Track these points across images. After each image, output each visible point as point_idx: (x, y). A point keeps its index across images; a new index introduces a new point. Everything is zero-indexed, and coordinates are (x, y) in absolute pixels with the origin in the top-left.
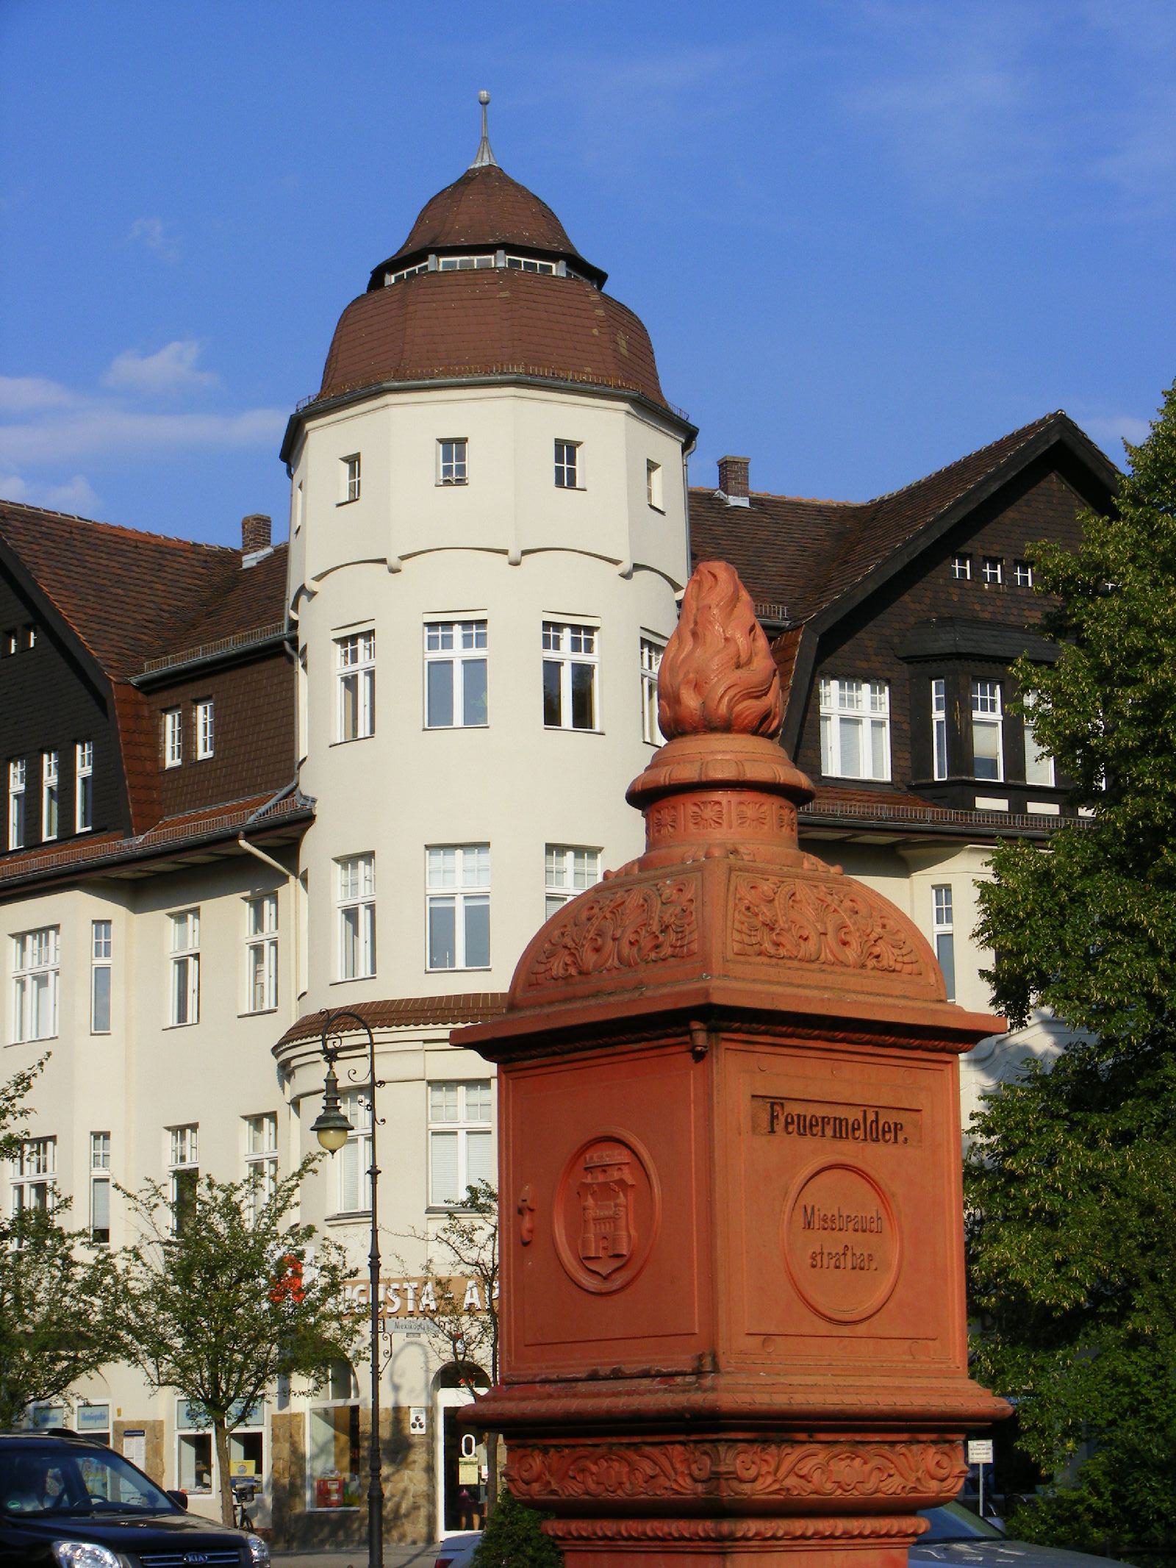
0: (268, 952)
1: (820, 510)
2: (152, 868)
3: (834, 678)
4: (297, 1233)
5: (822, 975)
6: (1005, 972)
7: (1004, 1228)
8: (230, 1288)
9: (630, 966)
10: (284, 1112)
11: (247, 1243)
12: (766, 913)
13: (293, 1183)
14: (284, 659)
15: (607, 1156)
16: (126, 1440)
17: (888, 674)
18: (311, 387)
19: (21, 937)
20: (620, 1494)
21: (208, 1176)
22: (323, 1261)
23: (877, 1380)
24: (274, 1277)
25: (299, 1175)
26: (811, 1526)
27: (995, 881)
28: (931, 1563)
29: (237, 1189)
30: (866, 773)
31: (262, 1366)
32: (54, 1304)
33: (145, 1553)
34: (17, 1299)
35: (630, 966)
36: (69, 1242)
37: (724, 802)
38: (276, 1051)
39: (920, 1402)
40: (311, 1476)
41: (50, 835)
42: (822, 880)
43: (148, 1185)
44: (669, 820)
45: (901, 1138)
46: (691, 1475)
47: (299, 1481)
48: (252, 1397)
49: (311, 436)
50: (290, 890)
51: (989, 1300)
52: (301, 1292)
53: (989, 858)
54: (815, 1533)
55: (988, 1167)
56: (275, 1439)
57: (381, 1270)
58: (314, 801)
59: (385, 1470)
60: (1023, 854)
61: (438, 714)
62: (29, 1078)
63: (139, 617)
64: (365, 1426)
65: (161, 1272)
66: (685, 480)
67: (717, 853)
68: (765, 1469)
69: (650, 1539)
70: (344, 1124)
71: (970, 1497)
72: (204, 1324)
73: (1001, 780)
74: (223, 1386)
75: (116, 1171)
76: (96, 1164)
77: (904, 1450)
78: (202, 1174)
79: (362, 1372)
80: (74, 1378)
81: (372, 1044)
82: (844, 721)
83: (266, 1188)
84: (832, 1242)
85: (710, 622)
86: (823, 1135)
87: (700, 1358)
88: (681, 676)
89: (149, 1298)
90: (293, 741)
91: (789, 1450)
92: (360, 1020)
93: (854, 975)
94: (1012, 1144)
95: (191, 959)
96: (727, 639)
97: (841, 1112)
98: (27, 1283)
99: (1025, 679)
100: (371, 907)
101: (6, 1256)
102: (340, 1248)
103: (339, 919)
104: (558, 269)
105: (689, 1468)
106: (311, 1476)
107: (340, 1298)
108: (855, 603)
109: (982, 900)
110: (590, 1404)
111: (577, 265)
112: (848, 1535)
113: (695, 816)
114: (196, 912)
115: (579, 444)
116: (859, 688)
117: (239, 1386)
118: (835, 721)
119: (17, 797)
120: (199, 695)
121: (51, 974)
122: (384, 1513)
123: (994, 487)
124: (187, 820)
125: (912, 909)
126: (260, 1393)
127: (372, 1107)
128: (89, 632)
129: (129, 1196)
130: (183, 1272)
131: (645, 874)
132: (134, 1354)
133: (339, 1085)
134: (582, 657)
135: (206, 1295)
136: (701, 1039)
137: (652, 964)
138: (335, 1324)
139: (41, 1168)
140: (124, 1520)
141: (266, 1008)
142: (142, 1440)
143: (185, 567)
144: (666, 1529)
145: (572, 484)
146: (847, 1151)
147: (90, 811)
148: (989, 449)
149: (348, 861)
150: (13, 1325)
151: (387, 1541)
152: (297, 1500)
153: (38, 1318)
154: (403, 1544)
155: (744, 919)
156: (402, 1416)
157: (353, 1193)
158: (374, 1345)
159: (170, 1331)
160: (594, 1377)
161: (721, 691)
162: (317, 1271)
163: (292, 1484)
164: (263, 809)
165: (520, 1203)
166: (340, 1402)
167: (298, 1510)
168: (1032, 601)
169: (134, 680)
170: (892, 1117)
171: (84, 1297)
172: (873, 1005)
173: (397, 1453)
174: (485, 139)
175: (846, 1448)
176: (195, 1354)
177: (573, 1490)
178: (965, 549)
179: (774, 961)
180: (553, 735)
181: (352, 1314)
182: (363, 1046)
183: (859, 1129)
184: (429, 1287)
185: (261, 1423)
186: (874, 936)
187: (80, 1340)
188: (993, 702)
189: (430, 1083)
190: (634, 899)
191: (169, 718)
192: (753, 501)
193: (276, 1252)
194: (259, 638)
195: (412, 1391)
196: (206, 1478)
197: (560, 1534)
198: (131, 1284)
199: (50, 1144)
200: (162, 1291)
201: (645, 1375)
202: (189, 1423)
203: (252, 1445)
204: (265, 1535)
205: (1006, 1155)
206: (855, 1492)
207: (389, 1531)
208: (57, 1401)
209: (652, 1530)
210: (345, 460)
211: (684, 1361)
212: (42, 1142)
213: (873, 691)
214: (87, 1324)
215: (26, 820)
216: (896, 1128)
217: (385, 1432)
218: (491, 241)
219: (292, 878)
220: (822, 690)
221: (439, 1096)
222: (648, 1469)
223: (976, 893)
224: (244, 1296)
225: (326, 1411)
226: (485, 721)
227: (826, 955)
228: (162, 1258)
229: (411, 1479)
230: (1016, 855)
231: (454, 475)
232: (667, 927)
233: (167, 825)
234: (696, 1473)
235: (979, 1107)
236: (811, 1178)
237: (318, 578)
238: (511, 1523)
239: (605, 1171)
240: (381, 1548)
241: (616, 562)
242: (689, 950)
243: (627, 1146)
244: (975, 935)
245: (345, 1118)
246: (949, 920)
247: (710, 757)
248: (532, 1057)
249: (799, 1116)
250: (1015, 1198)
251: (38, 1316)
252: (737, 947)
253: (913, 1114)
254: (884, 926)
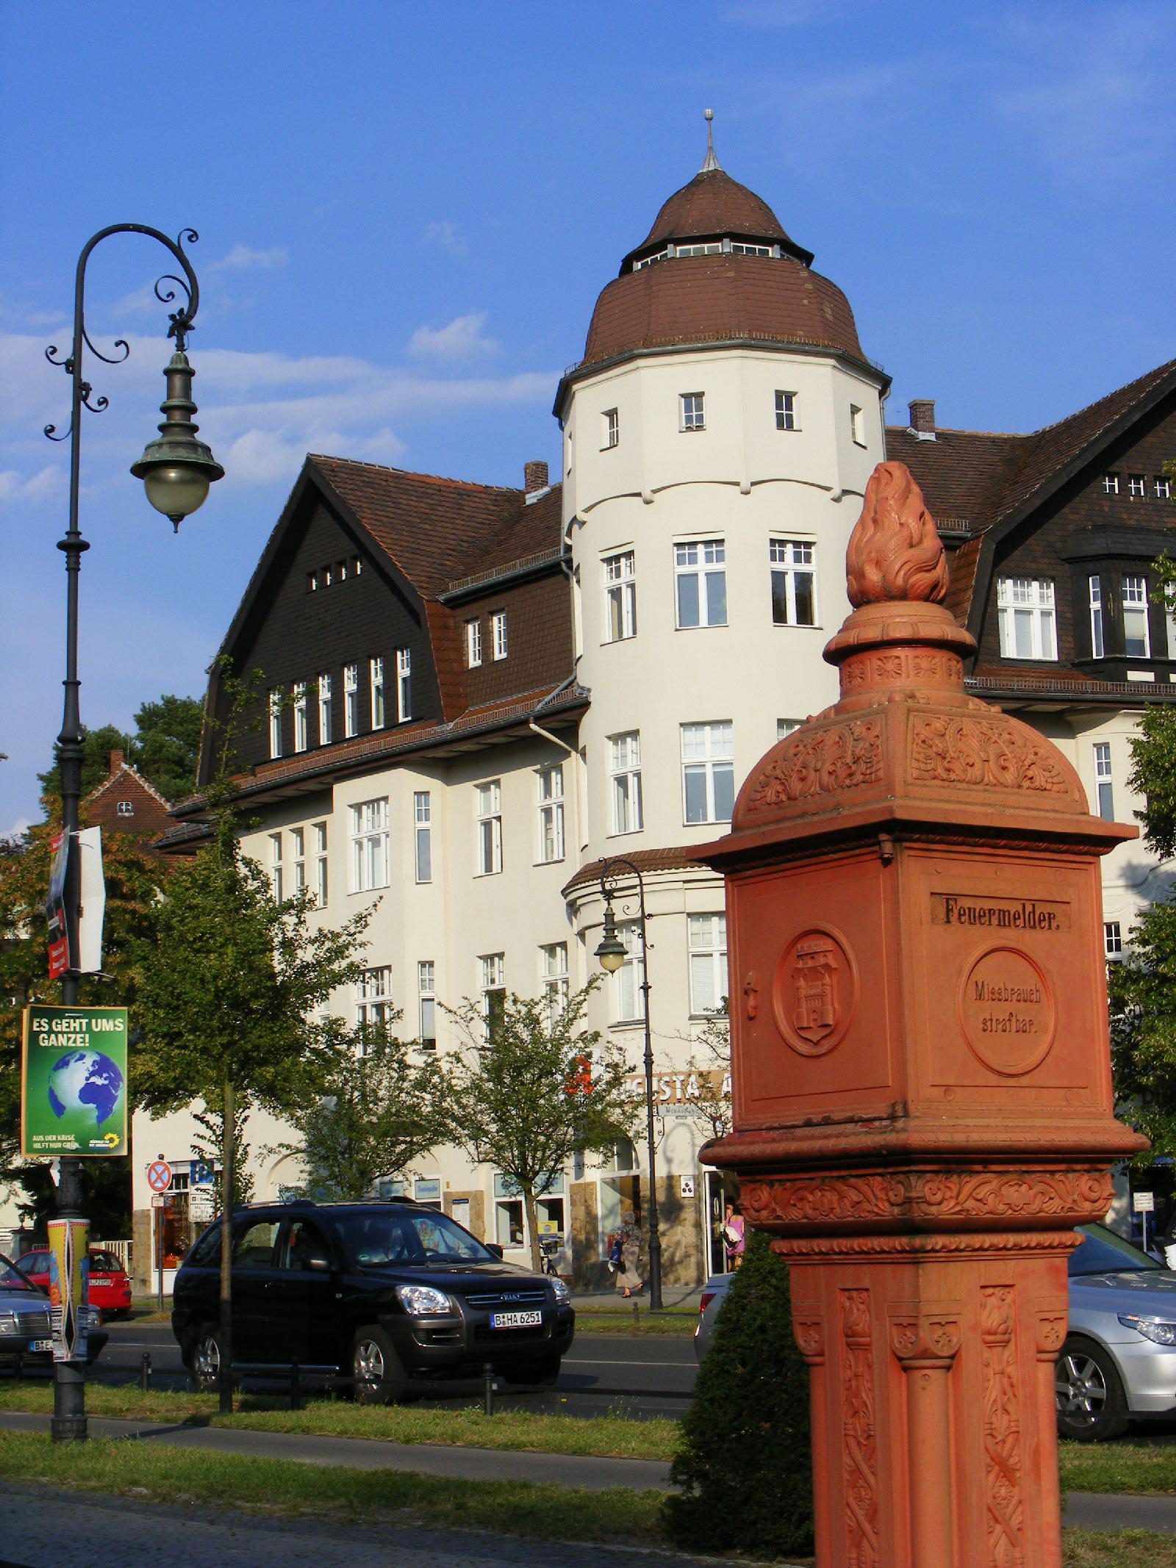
0: (556, 813)
1: (994, 441)
2: (460, 749)
3: (1009, 577)
4: (586, 1038)
5: (987, 795)
6: (1154, 812)
7: (1159, 1021)
8: (533, 1083)
9: (830, 791)
10: (573, 942)
11: (545, 1047)
12: (939, 744)
13: (582, 998)
14: (561, 577)
15: (815, 945)
16: (454, 1207)
17: (1053, 573)
18: (576, 356)
19: (357, 807)
20: (833, 1218)
21: (513, 994)
22: (608, 1060)
23: (1039, 1122)
24: (568, 1074)
25: (586, 991)
26: (988, 1240)
27: (1144, 739)
28: (1107, 1290)
29: (537, 1004)
30: (1037, 654)
31: (560, 1145)
32: (393, 1099)
33: (468, 1295)
34: (364, 1095)
35: (830, 791)
36: (403, 1050)
37: (903, 657)
38: (565, 893)
39: (1077, 1139)
40: (603, 1233)
41: (378, 724)
42: (984, 718)
43: (465, 1003)
44: (858, 671)
45: (1054, 925)
46: (888, 1200)
47: (592, 1237)
48: (553, 1171)
49: (577, 396)
50: (572, 763)
51: (1148, 1079)
52: (590, 1085)
53: (1139, 720)
54: (991, 1246)
55: (1144, 971)
56: (573, 1203)
57: (654, 1066)
58: (589, 690)
59: (662, 1227)
60: (1167, 716)
61: (687, 616)
62: (366, 917)
63: (443, 547)
64: (645, 1191)
65: (478, 1071)
66: (883, 420)
67: (897, 697)
68: (948, 1194)
69: (857, 1253)
70: (621, 949)
71: (1136, 1239)
72: (514, 1112)
73: (1148, 656)
74: (530, 1161)
75: (439, 992)
76: (423, 987)
77: (1062, 1178)
78: (508, 993)
79: (641, 1148)
80: (411, 1158)
81: (641, 885)
82: (1017, 612)
83: (560, 1002)
84: (1001, 1011)
85: (887, 511)
86: (990, 924)
87: (893, 1105)
88: (864, 556)
89: (468, 1093)
90: (571, 650)
91: (968, 1179)
92: (633, 867)
93: (1012, 794)
94: (1164, 952)
95: (494, 821)
96: (901, 525)
97: (1004, 905)
98: (371, 1083)
99: (1165, 572)
100: (638, 775)
101: (353, 1063)
102: (621, 1049)
103: (613, 785)
104: (773, 252)
105: (887, 1195)
106: (603, 1233)
107: (622, 1089)
108: (1024, 515)
109: (1134, 754)
110: (805, 1146)
111: (789, 248)
112: (1018, 1247)
113: (880, 668)
114: (497, 783)
115: (795, 394)
116: (1029, 585)
117: (543, 1161)
118: (1011, 612)
119: (351, 695)
120: (495, 608)
121: (383, 836)
122: (662, 1261)
123: (1136, 418)
124: (488, 709)
125: (1077, 758)
126: (560, 1166)
127: (642, 935)
128: (404, 560)
129: (450, 1011)
130: (495, 1071)
131: (840, 717)
132: (458, 1138)
133: (616, 919)
134: (803, 567)
135: (514, 1090)
136: (888, 848)
137: (846, 790)
138: (618, 1111)
139: (380, 991)
140: (453, 1268)
141: (556, 858)
142: (466, 1206)
143: (480, 505)
144: (870, 1245)
145: (790, 427)
146: (1011, 936)
147: (409, 704)
148: (1131, 387)
149: (618, 738)
150: (361, 1117)
151: (665, 1284)
152: (592, 1252)
153: (380, 1111)
154: (678, 1286)
155: (920, 750)
156: (674, 1183)
157: (631, 1006)
158: (650, 1126)
159: (486, 1118)
160: (809, 1124)
161: (897, 567)
162: (603, 1068)
163: (588, 1239)
164: (547, 699)
165: (746, 986)
166: (624, 1173)
167: (593, 1260)
168: (1169, 509)
169: (441, 598)
170: (1048, 908)
171: (417, 1093)
172: (1028, 817)
173: (672, 1213)
174: (711, 148)
175: (1015, 1176)
176: (507, 1137)
177: (794, 1215)
178: (1111, 469)
179: (946, 784)
180: (781, 631)
181: (631, 1102)
182: (634, 887)
183: (1019, 918)
184: (693, 1078)
185: (562, 1191)
186: (1028, 762)
187: (416, 1128)
188: (1140, 593)
189: (689, 915)
190: (832, 737)
191: (470, 627)
192: (938, 435)
193: (570, 1053)
194: (540, 560)
195: (681, 1162)
196: (519, 1236)
197: (785, 1251)
198: (454, 1082)
199: (386, 972)
200: (478, 1087)
201: (851, 1120)
202: (503, 1192)
203: (555, 1209)
204: (567, 1279)
205: (1159, 961)
206: (1022, 1212)
207: (666, 1275)
208: (397, 1176)
209: (859, 1246)
210: (606, 414)
211: (881, 1109)
212: (378, 972)
213: (1041, 587)
214: (420, 1114)
215: (359, 713)
216: (1049, 918)
217: (661, 1196)
218: (718, 231)
219: (573, 753)
220: (999, 588)
221: (697, 926)
222: (854, 1196)
223: (1130, 748)
224: (544, 1090)
225: (613, 1180)
226: (725, 621)
227: (989, 778)
228: (478, 1060)
229: (683, 1234)
230: (1162, 717)
231: (694, 423)
232: (858, 759)
233: (472, 713)
234: (893, 1199)
235: (1137, 922)
236: (982, 958)
237: (587, 510)
238: (758, 1259)
239: (813, 958)
240: (660, 1290)
241: (828, 489)
242: (876, 776)
243: (834, 939)
244: (1130, 783)
245: (622, 945)
246: (1108, 772)
247: (890, 621)
248: (752, 868)
249: (969, 909)
250: (1167, 995)
251: (380, 1108)
252: (915, 773)
253: (1064, 906)
254: (1036, 754)
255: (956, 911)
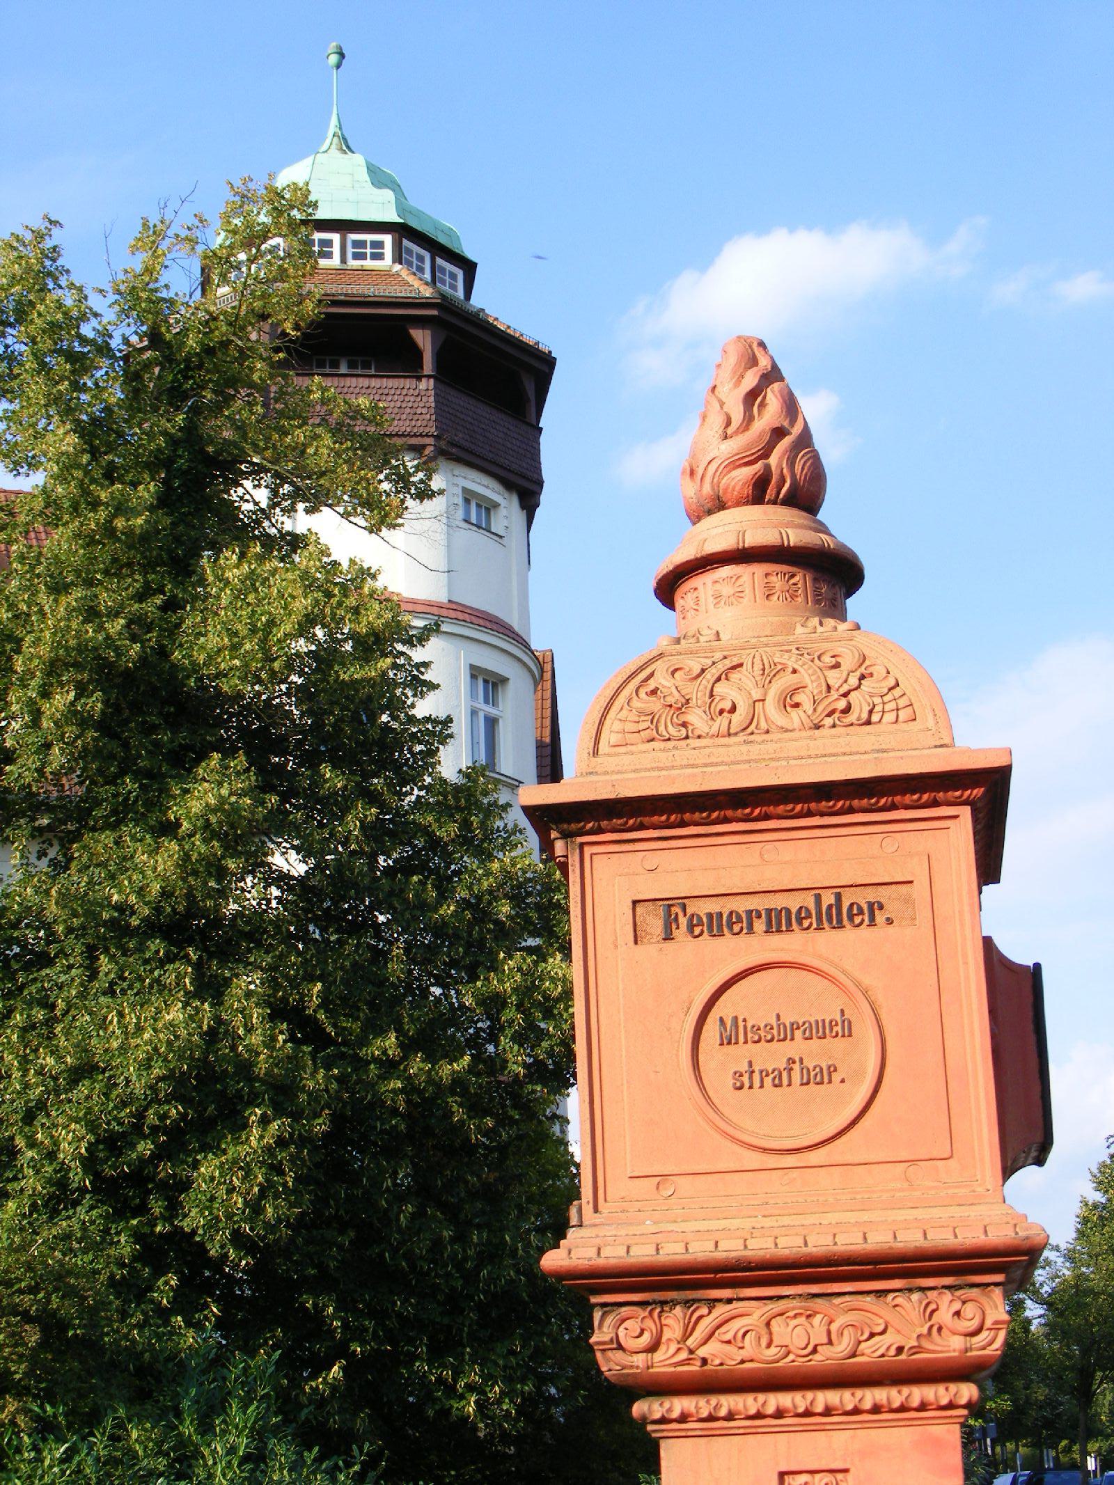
84: (771, 1057)
253: (904, 888)
255: (683, 921)
